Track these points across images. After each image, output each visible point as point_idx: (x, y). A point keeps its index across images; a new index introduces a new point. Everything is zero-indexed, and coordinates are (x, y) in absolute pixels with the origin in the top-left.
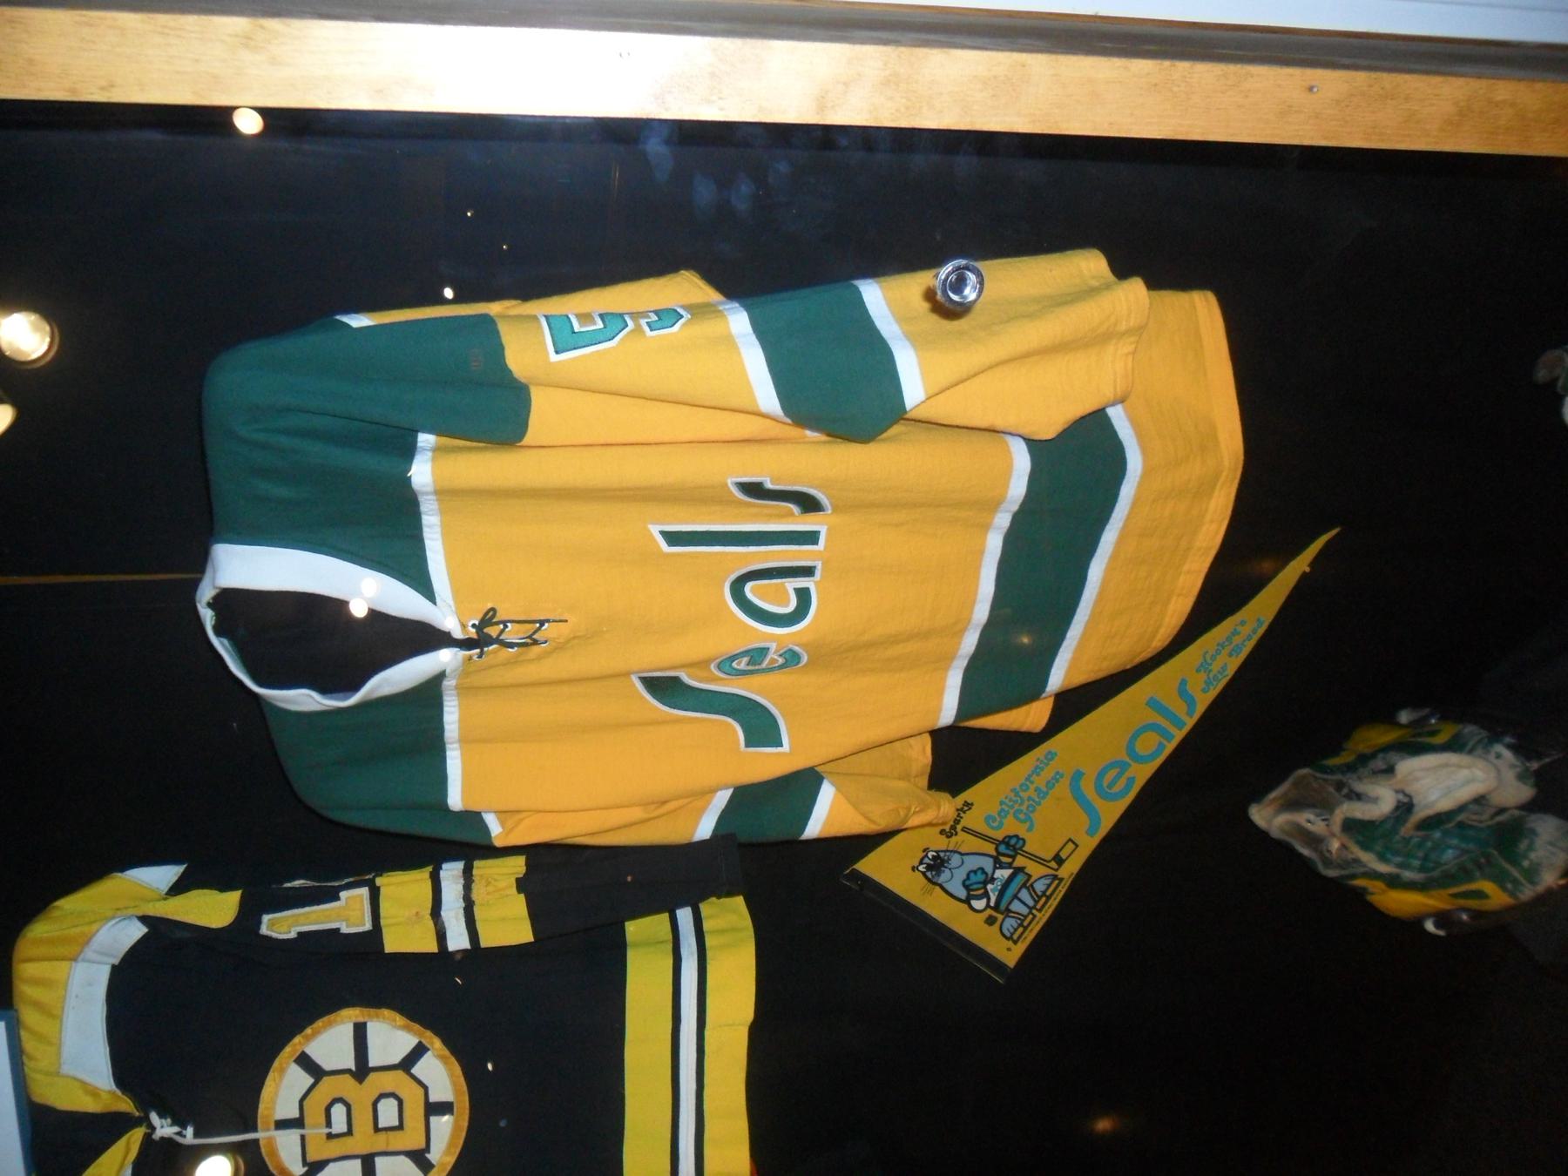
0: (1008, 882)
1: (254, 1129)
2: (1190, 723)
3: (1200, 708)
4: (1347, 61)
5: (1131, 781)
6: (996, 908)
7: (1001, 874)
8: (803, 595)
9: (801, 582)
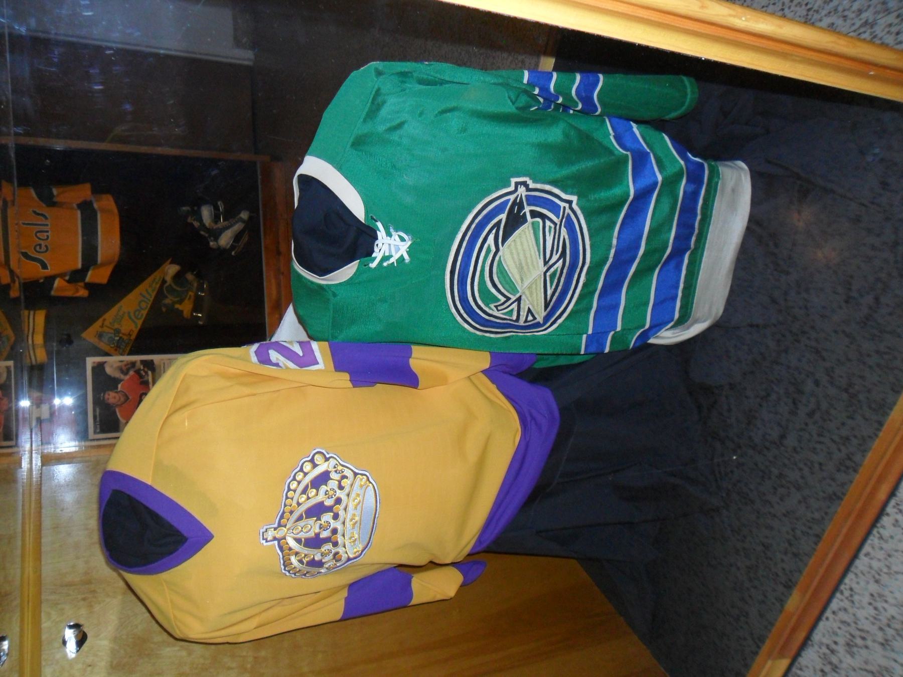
0: (118, 340)
1: (12, 52)
2: (151, 299)
3: (153, 297)
4: (460, 279)
5: (142, 315)
6: (117, 346)
7: (117, 338)
8: (48, 236)
9: (47, 234)
